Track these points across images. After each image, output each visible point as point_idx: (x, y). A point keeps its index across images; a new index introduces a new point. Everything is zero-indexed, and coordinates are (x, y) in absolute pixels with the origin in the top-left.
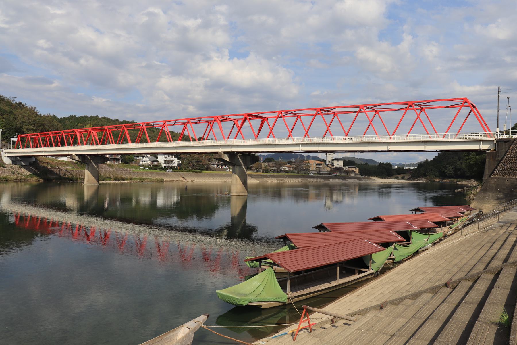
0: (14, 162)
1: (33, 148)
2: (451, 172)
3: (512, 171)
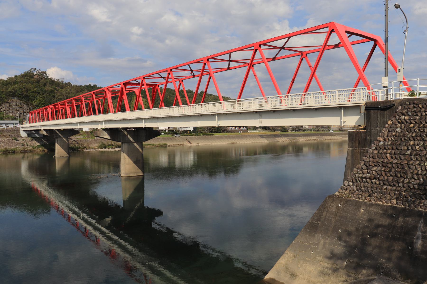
0: (29, 135)
1: (62, 119)
3: (379, 184)
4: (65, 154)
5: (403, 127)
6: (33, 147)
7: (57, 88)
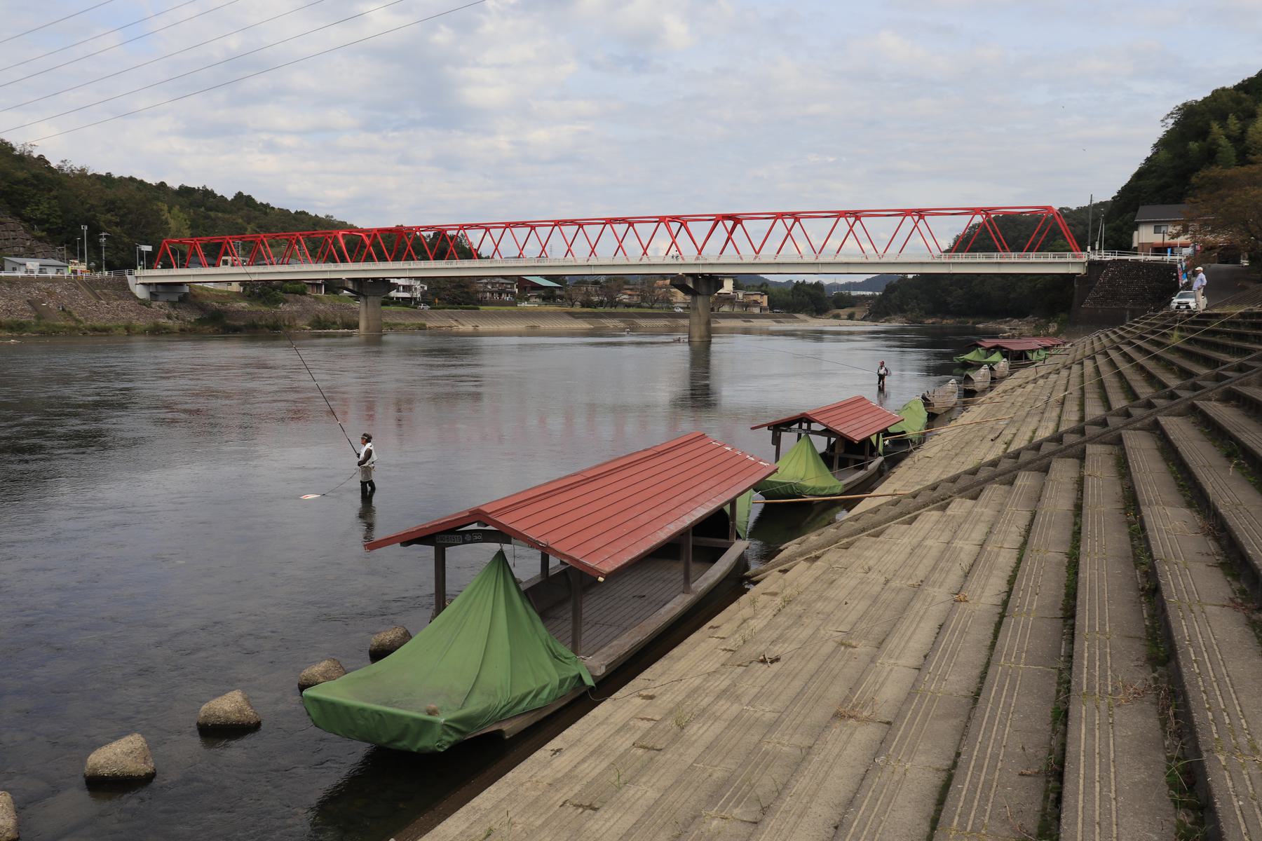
2: (961, 303)
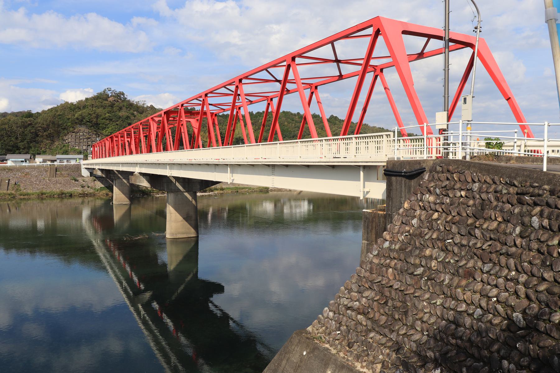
4: (126, 201)
5: (423, 218)
6: (95, 189)
7: (135, 113)
